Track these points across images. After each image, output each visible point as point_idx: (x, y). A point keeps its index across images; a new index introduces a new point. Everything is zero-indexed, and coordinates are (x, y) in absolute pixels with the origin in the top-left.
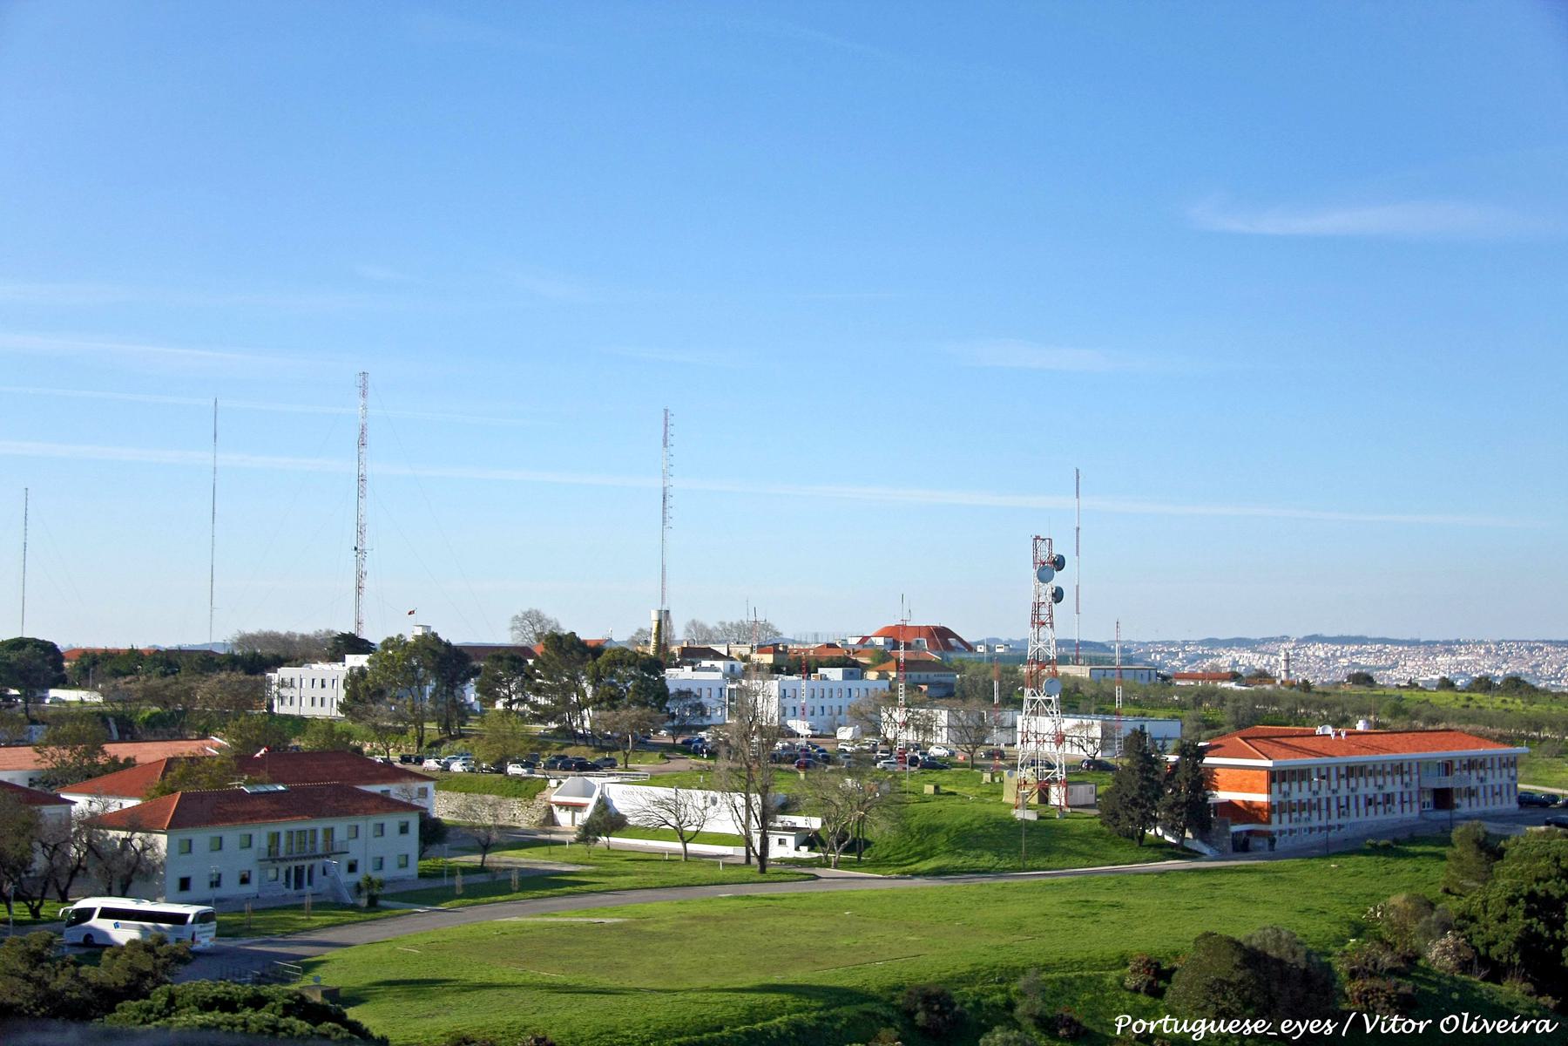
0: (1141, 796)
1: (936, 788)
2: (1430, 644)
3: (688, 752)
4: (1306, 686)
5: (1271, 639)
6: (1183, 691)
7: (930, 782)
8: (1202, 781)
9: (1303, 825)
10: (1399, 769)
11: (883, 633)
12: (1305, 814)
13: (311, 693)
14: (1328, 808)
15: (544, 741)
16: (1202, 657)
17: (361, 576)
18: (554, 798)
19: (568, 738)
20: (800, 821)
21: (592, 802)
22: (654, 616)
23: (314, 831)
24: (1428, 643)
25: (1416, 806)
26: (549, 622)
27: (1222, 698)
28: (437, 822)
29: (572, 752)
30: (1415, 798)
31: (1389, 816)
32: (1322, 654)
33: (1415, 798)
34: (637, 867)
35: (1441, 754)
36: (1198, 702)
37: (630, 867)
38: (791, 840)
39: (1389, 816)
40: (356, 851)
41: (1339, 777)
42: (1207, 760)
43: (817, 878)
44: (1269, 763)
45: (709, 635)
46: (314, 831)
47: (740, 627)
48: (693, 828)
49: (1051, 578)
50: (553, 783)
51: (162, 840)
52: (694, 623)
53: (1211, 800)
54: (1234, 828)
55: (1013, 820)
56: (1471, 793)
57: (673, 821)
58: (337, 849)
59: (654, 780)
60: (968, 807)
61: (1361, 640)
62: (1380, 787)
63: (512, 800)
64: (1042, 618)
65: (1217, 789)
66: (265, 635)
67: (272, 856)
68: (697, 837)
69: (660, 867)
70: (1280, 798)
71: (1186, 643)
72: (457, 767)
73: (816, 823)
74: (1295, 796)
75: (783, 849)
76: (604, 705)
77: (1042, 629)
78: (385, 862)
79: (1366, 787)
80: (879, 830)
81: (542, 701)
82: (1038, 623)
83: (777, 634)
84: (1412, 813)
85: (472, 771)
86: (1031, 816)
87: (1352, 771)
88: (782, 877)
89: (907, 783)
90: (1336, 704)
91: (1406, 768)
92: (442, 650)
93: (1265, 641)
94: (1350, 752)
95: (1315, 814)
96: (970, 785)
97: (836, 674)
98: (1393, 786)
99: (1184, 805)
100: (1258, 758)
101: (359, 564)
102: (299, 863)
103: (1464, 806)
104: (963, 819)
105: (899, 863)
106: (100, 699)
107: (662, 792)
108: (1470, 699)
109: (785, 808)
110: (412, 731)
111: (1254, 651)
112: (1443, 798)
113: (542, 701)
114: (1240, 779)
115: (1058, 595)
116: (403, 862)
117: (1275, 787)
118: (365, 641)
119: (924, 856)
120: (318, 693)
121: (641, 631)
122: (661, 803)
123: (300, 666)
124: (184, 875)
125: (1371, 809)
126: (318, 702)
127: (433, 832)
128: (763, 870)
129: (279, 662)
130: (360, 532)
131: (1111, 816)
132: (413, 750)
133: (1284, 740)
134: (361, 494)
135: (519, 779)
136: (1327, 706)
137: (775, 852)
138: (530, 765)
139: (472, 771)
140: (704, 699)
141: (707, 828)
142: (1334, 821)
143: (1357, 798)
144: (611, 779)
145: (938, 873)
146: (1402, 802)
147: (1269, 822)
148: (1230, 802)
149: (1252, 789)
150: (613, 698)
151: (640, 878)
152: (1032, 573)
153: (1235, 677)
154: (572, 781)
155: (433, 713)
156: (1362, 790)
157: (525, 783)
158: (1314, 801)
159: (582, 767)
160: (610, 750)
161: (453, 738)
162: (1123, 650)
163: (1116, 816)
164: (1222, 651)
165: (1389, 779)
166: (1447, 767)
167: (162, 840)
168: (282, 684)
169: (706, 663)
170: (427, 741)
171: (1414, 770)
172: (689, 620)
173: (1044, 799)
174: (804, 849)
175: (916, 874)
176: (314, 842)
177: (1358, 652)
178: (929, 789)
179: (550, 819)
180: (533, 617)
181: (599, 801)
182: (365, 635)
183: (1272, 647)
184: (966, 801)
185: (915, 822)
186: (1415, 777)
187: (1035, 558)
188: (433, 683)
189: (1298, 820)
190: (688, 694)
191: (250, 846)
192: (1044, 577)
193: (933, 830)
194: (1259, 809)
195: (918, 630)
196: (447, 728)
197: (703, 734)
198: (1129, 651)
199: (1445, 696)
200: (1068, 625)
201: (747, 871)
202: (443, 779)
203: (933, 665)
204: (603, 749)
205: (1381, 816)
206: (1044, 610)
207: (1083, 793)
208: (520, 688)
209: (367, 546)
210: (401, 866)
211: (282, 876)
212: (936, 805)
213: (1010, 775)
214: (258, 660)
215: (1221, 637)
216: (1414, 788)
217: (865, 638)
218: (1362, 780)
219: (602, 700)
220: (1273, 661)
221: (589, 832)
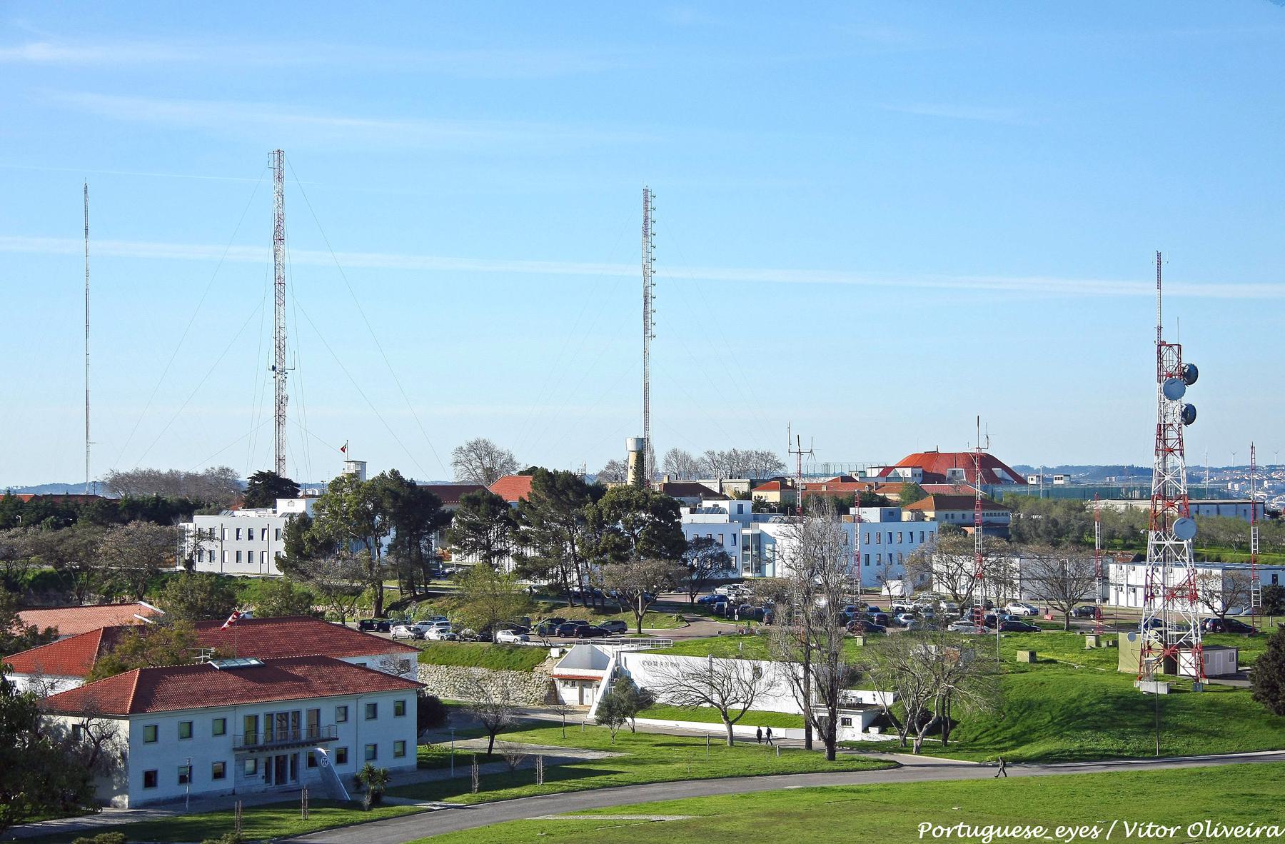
1: (1032, 654)
3: (711, 613)
7: (1021, 648)
11: (914, 461)
13: (242, 547)
15: (531, 599)
17: (280, 403)
18: (557, 671)
19: (558, 597)
20: (867, 697)
21: (606, 674)
22: (631, 445)
23: (297, 714)
26: (501, 455)
28: (434, 700)
29: (569, 613)
34: (675, 753)
37: (665, 753)
38: (857, 720)
40: (346, 736)
43: (899, 766)
45: (694, 469)
46: (297, 714)
47: (733, 457)
48: (740, 706)
50: (555, 652)
51: (123, 726)
52: (675, 453)
55: (1136, 693)
57: (716, 698)
58: (325, 736)
59: (677, 648)
60: (1078, 677)
63: (505, 673)
64: (1170, 444)
66: (143, 473)
67: (249, 746)
68: (741, 717)
69: (705, 754)
72: (432, 634)
73: (888, 699)
75: (852, 731)
76: (607, 556)
77: (1170, 456)
78: (379, 749)
80: (971, 707)
81: (530, 552)
83: (780, 466)
85: (452, 639)
86: (1162, 690)
88: (857, 765)
89: (518, 637)
92: (405, 492)
96: (1071, 650)
97: (872, 515)
101: (279, 389)
102: (281, 752)
104: (1073, 694)
105: (998, 745)
107: (700, 663)
109: (854, 679)
110: (369, 592)
113: (530, 552)
115: (1189, 415)
116: (399, 749)
118: (288, 482)
119: (1020, 740)
120: (245, 546)
121: (613, 464)
122: (697, 676)
123: (217, 512)
124: (150, 767)
126: (245, 557)
127: (433, 716)
128: (832, 757)
129: (188, 510)
130: (279, 348)
132: (370, 614)
134: (279, 301)
135: (512, 648)
137: (844, 734)
138: (521, 630)
139: (452, 639)
140: (728, 547)
141: (757, 706)
144: (625, 647)
145: (1044, 759)
150: (618, 547)
151: (684, 766)
152: (1156, 387)
154: (579, 650)
155: (395, 567)
157: (518, 654)
159: (586, 632)
160: (617, 611)
161: (418, 599)
162: (1190, 479)
167: (123, 726)
168: (200, 535)
169: (707, 504)
170: (386, 603)
172: (670, 449)
173: (1171, 665)
174: (874, 731)
175: (1017, 761)
176: (298, 726)
178: (1023, 656)
179: (553, 697)
180: (481, 449)
181: (615, 674)
182: (288, 474)
184: (1073, 669)
185: (1013, 696)
188: (393, 532)
190: (709, 541)
191: (224, 732)
193: (1028, 707)
195: (952, 458)
196: (410, 586)
197: (722, 591)
198: (1199, 480)
200: (1208, 449)
201: (811, 758)
202: (429, 654)
203: (972, 497)
204: (604, 610)
208: (501, 536)
209: (288, 365)
210: (397, 755)
211: (262, 765)
212: (1035, 675)
213: (1132, 638)
214: (161, 506)
217: (887, 470)
219: (605, 551)
221: (612, 711)
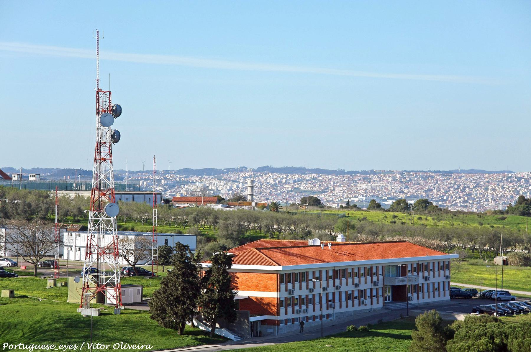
0: (183, 295)
2: (352, 173)
4: (276, 207)
5: (233, 170)
6: (186, 212)
8: (228, 283)
9: (302, 315)
10: (370, 271)
12: (304, 307)
14: (321, 302)
16: (180, 183)
24: (351, 173)
25: (381, 299)
27: (216, 217)
30: (380, 293)
31: (362, 307)
32: (271, 181)
33: (380, 293)
35: (399, 260)
36: (196, 221)
39: (362, 307)
41: (328, 278)
42: (234, 267)
44: (279, 268)
49: (111, 123)
53: (236, 298)
54: (252, 319)
55: (79, 316)
56: (418, 289)
60: (41, 307)
61: (301, 170)
62: (357, 285)
64: (104, 155)
65: (237, 288)
70: (286, 295)
71: (167, 172)
74: (297, 294)
77: (104, 163)
79: (347, 286)
82: (99, 159)
84: (378, 305)
87: (337, 274)
90: (301, 222)
91: (374, 271)
93: (228, 171)
94: (335, 259)
95: (311, 306)
96: (37, 289)
98: (366, 284)
99: (216, 301)
100: (273, 265)
103: (415, 300)
104: (38, 318)
106: (210, 265)
108: (395, 217)
111: (220, 179)
112: (399, 293)
114: (256, 281)
115: (116, 137)
117: (283, 286)
125: (350, 302)
131: (160, 312)
133: (288, 250)
136: (295, 223)
142: (325, 312)
143: (340, 293)
146: (372, 296)
147: (278, 313)
148: (249, 299)
149: (266, 289)
153: (220, 200)
156: (344, 288)
158: (310, 296)
162: (116, 178)
163: (164, 311)
164: (195, 178)
165: (363, 279)
166: (403, 270)
171: (380, 272)
173: (101, 298)
177: (299, 180)
183: (234, 176)
186: (381, 277)
187: (98, 107)
189: (299, 312)
192: (105, 123)
194: (268, 304)
198: (122, 179)
199: (374, 215)
200: (129, 160)
205: (357, 308)
206: (105, 149)
207: (132, 294)
213: (77, 281)
215: (194, 168)
216: (380, 285)
218: (344, 280)
220: (234, 187)
